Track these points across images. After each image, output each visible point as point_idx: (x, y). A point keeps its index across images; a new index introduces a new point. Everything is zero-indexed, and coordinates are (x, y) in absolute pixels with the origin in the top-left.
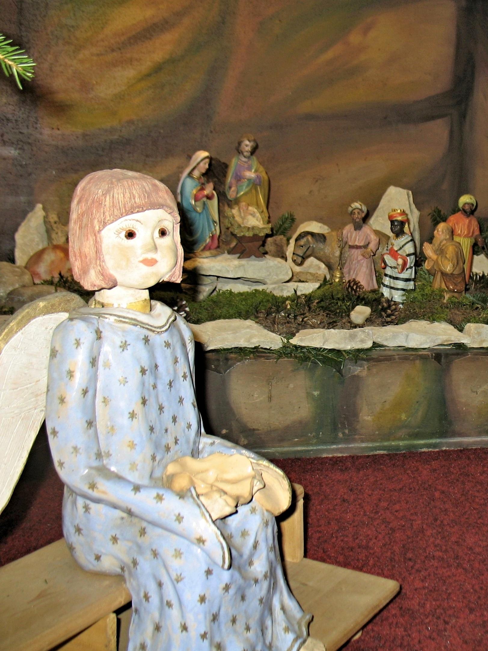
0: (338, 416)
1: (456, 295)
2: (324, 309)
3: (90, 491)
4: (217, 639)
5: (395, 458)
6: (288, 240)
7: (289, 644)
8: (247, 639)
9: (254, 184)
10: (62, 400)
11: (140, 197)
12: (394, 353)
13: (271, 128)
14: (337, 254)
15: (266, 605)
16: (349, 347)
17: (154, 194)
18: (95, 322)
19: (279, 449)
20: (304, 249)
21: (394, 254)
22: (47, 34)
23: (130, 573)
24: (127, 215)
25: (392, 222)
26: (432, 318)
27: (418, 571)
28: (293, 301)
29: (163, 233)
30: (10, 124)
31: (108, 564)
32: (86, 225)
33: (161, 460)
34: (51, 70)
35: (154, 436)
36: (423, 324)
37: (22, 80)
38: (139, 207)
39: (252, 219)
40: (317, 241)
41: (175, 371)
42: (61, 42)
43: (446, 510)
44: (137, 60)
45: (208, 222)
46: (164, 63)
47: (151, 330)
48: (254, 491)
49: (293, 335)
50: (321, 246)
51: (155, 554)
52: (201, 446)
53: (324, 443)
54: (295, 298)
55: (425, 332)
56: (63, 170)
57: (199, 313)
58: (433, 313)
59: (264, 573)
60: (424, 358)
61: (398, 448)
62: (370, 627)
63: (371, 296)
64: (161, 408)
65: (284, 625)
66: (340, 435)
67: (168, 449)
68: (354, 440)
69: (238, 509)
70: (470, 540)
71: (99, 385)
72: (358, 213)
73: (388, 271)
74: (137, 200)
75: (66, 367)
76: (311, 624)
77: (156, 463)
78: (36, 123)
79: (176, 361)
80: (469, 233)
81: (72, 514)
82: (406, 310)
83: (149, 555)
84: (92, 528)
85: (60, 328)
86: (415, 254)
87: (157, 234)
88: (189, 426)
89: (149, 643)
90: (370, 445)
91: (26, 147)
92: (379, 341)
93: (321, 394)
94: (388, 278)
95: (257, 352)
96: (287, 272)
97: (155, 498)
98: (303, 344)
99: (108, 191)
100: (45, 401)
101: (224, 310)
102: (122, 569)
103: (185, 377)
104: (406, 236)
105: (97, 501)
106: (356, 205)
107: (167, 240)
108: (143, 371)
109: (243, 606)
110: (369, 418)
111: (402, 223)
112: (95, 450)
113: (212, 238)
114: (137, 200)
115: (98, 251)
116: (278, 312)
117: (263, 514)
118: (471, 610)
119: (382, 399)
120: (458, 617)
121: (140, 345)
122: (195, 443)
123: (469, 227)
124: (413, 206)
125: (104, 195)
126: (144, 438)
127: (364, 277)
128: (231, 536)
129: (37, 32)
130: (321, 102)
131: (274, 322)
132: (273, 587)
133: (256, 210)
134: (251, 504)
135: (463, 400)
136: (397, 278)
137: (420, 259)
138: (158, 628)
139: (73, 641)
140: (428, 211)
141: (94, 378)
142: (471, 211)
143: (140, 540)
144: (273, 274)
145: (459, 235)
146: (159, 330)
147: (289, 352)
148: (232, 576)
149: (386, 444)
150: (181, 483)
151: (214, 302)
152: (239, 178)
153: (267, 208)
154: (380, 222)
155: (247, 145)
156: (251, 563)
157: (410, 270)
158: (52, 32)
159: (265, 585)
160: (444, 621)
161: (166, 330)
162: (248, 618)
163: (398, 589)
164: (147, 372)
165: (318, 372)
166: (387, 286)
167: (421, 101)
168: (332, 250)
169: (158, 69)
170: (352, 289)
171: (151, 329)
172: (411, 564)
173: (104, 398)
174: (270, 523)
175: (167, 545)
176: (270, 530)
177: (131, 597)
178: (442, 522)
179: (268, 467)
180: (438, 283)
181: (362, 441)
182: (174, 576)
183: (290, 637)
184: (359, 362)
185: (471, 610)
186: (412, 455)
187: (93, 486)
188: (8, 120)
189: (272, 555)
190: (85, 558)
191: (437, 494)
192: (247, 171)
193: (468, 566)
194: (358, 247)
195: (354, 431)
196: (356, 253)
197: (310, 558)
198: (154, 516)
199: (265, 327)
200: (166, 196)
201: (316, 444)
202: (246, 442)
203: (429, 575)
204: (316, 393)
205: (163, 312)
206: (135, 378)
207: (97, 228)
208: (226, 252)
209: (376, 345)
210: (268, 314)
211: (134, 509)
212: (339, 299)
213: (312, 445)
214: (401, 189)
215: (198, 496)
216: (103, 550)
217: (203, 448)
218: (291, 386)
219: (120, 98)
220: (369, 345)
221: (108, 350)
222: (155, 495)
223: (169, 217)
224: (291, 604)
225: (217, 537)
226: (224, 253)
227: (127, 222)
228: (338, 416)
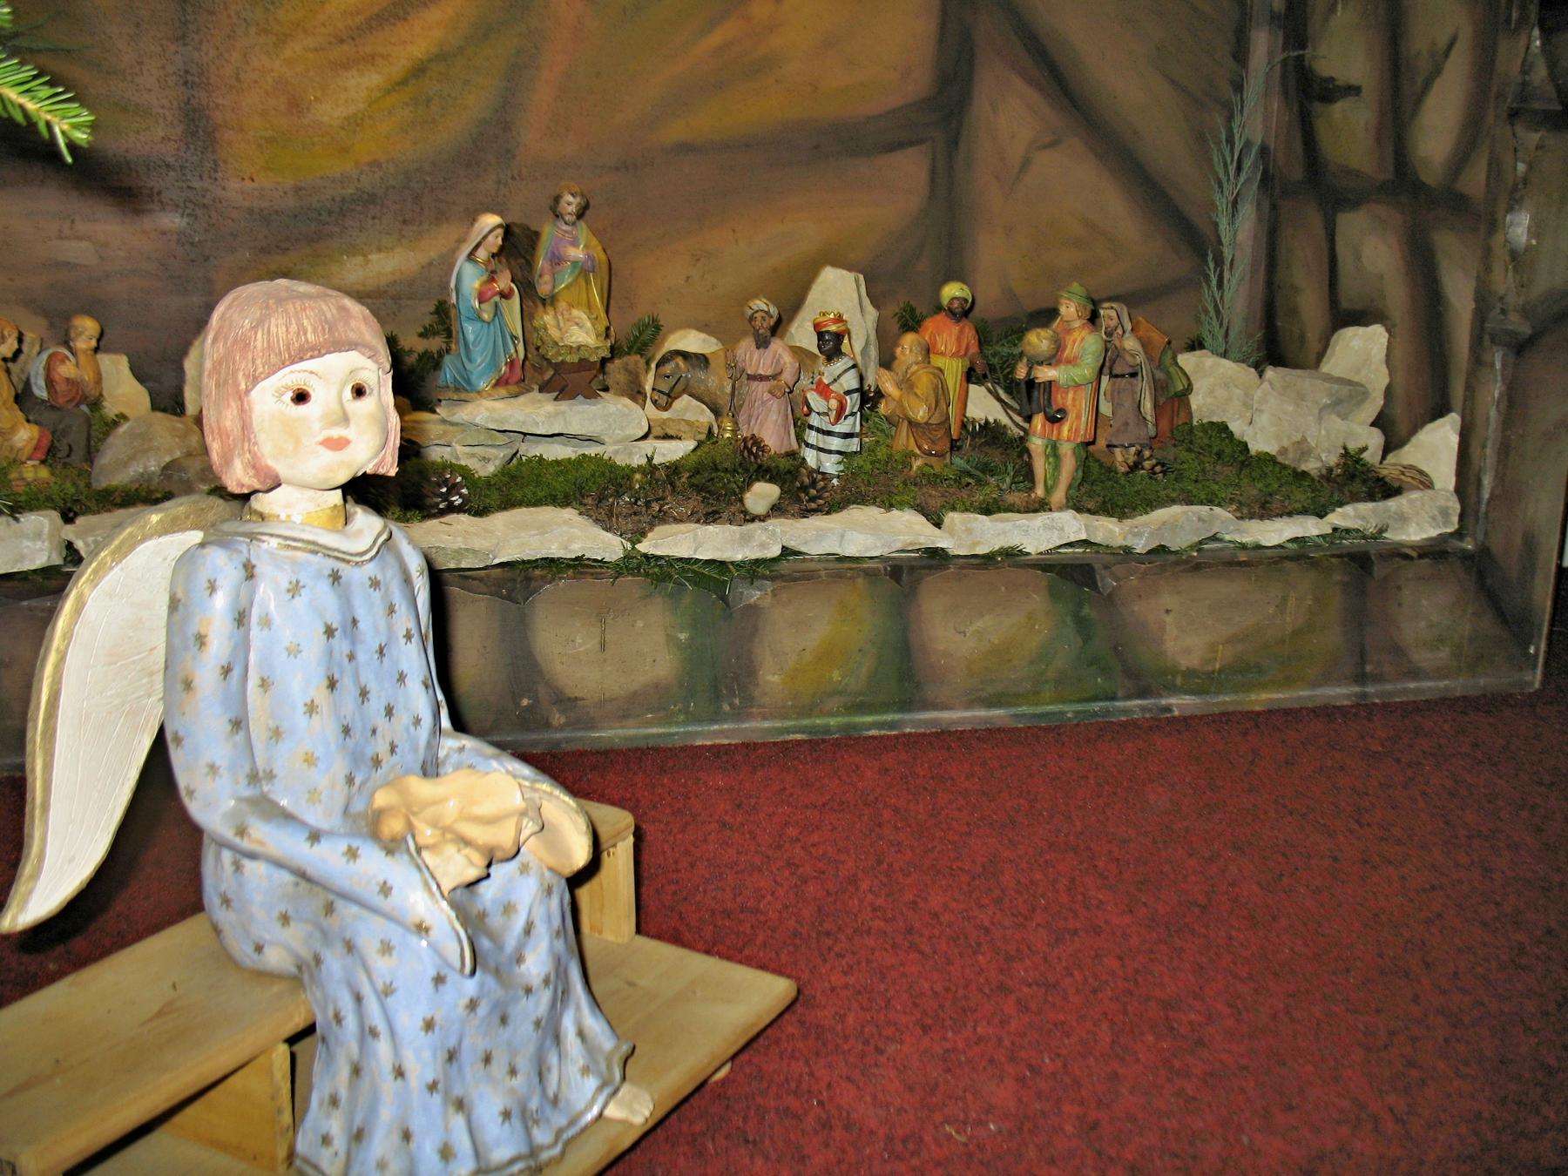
0: (720, 676)
1: (933, 460)
2: (699, 488)
3: (237, 840)
4: (457, 1091)
5: (819, 747)
6: (648, 363)
7: (589, 1095)
8: (512, 1091)
9: (584, 271)
10: (188, 685)
11: (315, 331)
12: (819, 566)
13: (617, 169)
14: (729, 389)
15: (550, 1030)
16: (739, 557)
17: (340, 326)
18: (244, 548)
19: (620, 732)
20: (672, 381)
21: (824, 391)
22: (229, 17)
23: (311, 975)
24: (293, 363)
25: (820, 335)
26: (888, 503)
27: (840, 956)
28: (644, 474)
29: (359, 392)
30: (172, 174)
31: (275, 958)
32: (226, 382)
33: (364, 783)
34: (238, 79)
35: (350, 742)
36: (872, 513)
37: (72, 146)
38: (312, 349)
39: (577, 331)
41: (390, 628)
42: (253, 30)
43: (899, 844)
44: (382, 56)
45: (503, 337)
46: (430, 60)
47: (343, 560)
48: (522, 838)
49: (643, 534)
50: (702, 375)
51: (350, 947)
52: (442, 754)
53: (700, 721)
54: (650, 468)
55: (874, 529)
56: (262, 250)
57: (486, 496)
58: (890, 494)
59: (542, 976)
60: (870, 574)
62: (744, 1057)
63: (784, 464)
64: (364, 694)
65: (581, 1062)
66: (726, 707)
67: (377, 762)
68: (750, 717)
69: (493, 870)
70: (936, 901)
71: (253, 658)
73: (814, 420)
74: (311, 337)
75: (193, 629)
76: (630, 1062)
77: (355, 789)
78: (216, 171)
79: (391, 610)
81: (217, 872)
82: (843, 490)
83: (339, 948)
84: (249, 896)
85: (186, 561)
86: (860, 390)
87: (348, 393)
88: (417, 722)
89: (343, 1094)
90: (778, 724)
91: (199, 212)
92: (792, 544)
93: (692, 638)
94: (814, 433)
95: (579, 566)
97: (345, 854)
98: (659, 553)
99: (260, 322)
100: (159, 686)
101: (528, 491)
102: (299, 968)
103: (408, 637)
104: (845, 359)
105: (252, 856)
106: (759, 304)
107: (367, 404)
108: (330, 632)
109: (505, 1034)
110: (776, 678)
111: (838, 337)
112: (247, 768)
113: (511, 365)
114: (311, 337)
115: (246, 426)
116: (618, 495)
117: (542, 875)
118: (926, 1029)
119: (799, 648)
120: (902, 1042)
121: (324, 586)
122: (429, 745)
123: (959, 340)
124: (867, 302)
125: (254, 328)
126: (333, 747)
127: (773, 434)
128: (483, 915)
129: (211, 13)
130: (704, 122)
131: (610, 515)
132: (561, 997)
133: (584, 316)
134: (519, 858)
136: (829, 433)
137: (869, 399)
138: (356, 1071)
139: (221, 1087)
140: (893, 308)
141: (244, 646)
142: (963, 312)
143: (325, 922)
144: (615, 428)
145: (942, 354)
146: (358, 559)
148: (482, 985)
149: (806, 722)
150: (393, 826)
151: (513, 477)
152: (556, 260)
153: (607, 312)
154: (802, 334)
155: (570, 203)
156: (520, 960)
157: (851, 419)
158: (238, 14)
159: (545, 997)
160: (877, 1049)
161: (372, 559)
162: (513, 1052)
163: (793, 993)
164: (337, 634)
165: (687, 600)
166: (812, 446)
168: (716, 381)
169: (419, 71)
170: (750, 452)
171: (343, 558)
172: (829, 942)
173: (263, 680)
174: (555, 889)
175: (369, 931)
176: (555, 902)
177: (314, 1015)
178: (890, 865)
179: (551, 794)
180: (903, 440)
181: (765, 718)
182: (380, 986)
183: (592, 1083)
184: (757, 583)
185: (926, 1029)
186: (850, 742)
187: (242, 831)
188: (168, 166)
189: (560, 945)
190: (242, 949)
191: (887, 814)
192: (571, 247)
193: (927, 949)
194: (762, 378)
195: (749, 700)
196: (760, 388)
197: (659, 937)
198: (345, 884)
199: (597, 521)
200: (363, 328)
202: (563, 720)
203: (859, 963)
204: (683, 636)
205: (367, 524)
206: (314, 644)
207: (243, 386)
208: (536, 387)
209: (786, 552)
210: (601, 499)
211: (310, 871)
212: (726, 470)
213: (677, 724)
214: (844, 272)
215: (419, 850)
216: (267, 937)
217: (447, 756)
218: (640, 624)
219: (355, 123)
220: (775, 551)
221: (267, 594)
222: (344, 848)
223: (370, 364)
224: (595, 1025)
225: (450, 922)
226: (529, 390)
227: (292, 376)
228: (720, 676)
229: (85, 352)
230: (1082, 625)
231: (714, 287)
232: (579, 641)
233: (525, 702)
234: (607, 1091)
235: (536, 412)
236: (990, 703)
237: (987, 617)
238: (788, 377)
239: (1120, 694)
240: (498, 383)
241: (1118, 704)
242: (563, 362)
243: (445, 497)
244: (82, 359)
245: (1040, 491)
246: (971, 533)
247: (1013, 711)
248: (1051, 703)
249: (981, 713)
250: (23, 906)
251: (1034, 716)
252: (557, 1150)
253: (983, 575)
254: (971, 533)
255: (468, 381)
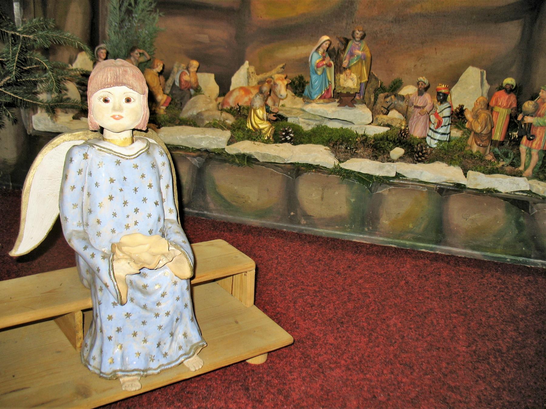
0: (366, 218)
5: (400, 252)
9: (362, 59)
16: (377, 174)
24: (101, 89)
39: (350, 82)
40: (398, 100)
53: (355, 232)
61: (405, 245)
66: (366, 229)
67: (127, 227)
68: (375, 235)
72: (422, 84)
80: (507, 106)
90: (386, 239)
94: (431, 131)
95: (317, 168)
96: (368, 118)
113: (328, 91)
124: (485, 82)
135: (455, 223)
144: (361, 120)
146: (128, 157)
147: (338, 171)
149: (397, 241)
152: (352, 55)
155: (358, 34)
161: (134, 158)
165: (355, 187)
167: (503, 6)
170: (402, 135)
181: (381, 236)
192: (359, 49)
196: (418, 110)
201: (349, 232)
202: (305, 223)
204: (353, 200)
209: (398, 176)
213: (347, 232)
218: (337, 193)
220: (393, 174)
228: (366, 218)
229: (193, 72)
230: (520, 226)
231: (425, 70)
232: (314, 195)
233: (292, 214)
234: (186, 356)
235: (331, 110)
236: (473, 248)
237: (477, 215)
238: (427, 108)
239: (532, 256)
240: (320, 98)
241: (532, 260)
242: (341, 92)
243: (284, 136)
244: (191, 74)
245: (521, 168)
246: (478, 180)
247: (483, 253)
248: (501, 254)
249: (469, 251)
250: (16, 251)
251: (493, 257)
252: (156, 372)
253: (477, 198)
254: (478, 180)
255: (311, 96)
